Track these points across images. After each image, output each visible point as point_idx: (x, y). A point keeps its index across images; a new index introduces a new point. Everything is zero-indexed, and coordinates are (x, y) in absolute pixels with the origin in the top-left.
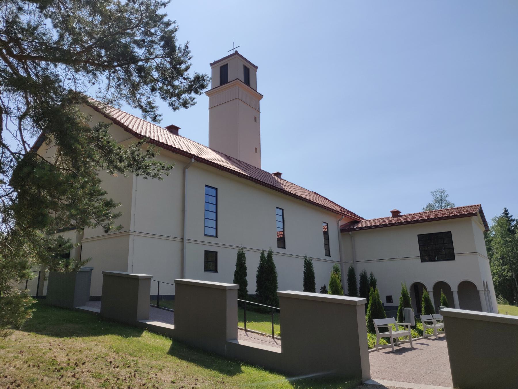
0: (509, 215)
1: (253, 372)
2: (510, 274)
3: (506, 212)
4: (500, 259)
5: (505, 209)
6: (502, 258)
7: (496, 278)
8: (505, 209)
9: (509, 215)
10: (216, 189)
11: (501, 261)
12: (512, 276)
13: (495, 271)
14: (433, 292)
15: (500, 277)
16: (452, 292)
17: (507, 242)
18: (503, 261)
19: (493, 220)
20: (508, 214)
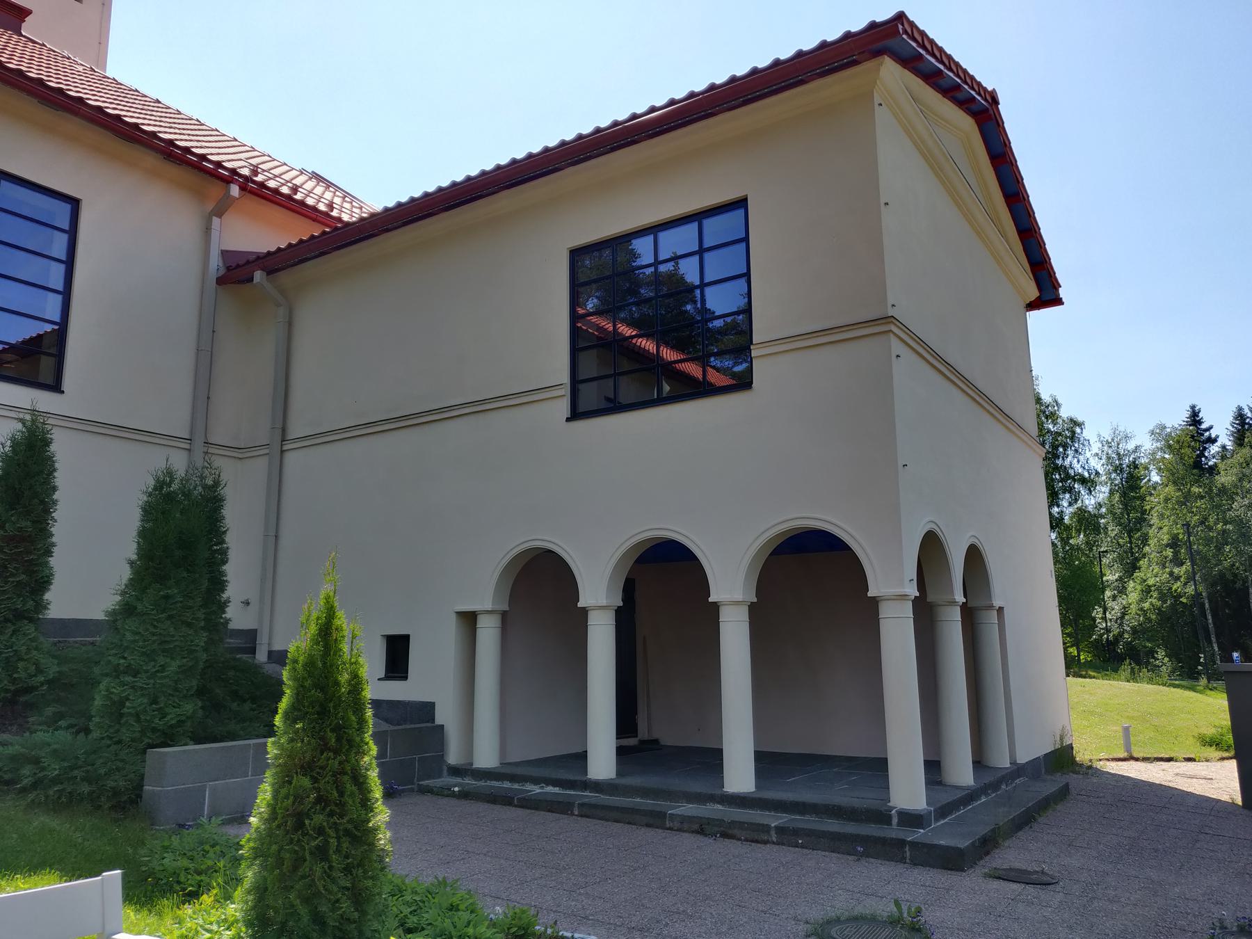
0: (1204, 426)
1: (1210, 700)
2: (1190, 590)
3: (1195, 418)
4: (1167, 546)
5: (1193, 407)
6: (1174, 543)
7: (1154, 600)
8: (1193, 407)
9: (1204, 426)
10: (75, 203)
11: (1169, 553)
12: (1198, 595)
13: (1151, 582)
14: (753, 609)
15: (1162, 597)
16: (716, 607)
17: (1187, 499)
18: (1176, 554)
19: (1152, 433)
20: (1200, 422)
